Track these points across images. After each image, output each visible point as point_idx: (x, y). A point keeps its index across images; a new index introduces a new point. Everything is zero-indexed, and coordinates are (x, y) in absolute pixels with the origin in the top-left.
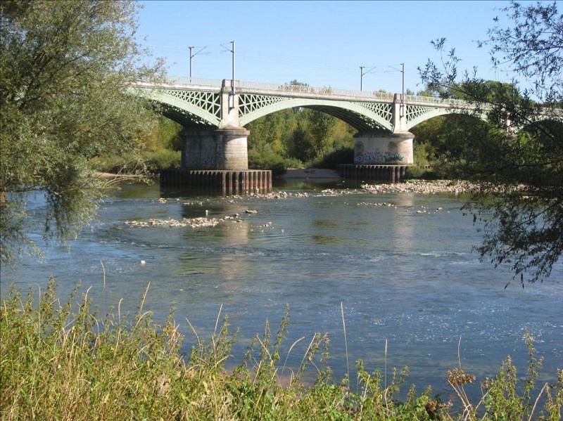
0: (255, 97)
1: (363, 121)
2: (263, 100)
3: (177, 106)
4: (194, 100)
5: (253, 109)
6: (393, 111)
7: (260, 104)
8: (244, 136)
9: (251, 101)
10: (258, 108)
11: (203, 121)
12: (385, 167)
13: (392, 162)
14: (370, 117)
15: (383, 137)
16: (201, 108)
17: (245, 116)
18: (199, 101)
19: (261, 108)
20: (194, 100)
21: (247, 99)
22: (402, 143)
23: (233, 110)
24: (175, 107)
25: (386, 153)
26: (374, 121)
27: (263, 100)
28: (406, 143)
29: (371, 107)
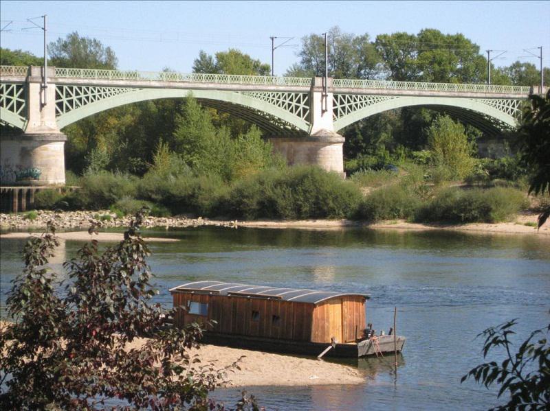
0: (351, 97)
1: (489, 121)
2: (360, 100)
3: (261, 110)
4: (280, 102)
5: (349, 112)
6: (310, 103)
7: (362, 104)
8: (338, 142)
9: (346, 102)
10: (360, 107)
11: (290, 125)
12: (5, 189)
13: (24, 181)
14: (497, 117)
15: (12, 139)
16: (288, 111)
17: (339, 120)
18: (505, 108)
19: (358, 110)
20: (280, 102)
21: (341, 100)
22: (38, 149)
23: (326, 113)
24: (259, 111)
25: (17, 166)
26: (503, 123)
27: (360, 100)
28: (46, 149)
29: (498, 104)
